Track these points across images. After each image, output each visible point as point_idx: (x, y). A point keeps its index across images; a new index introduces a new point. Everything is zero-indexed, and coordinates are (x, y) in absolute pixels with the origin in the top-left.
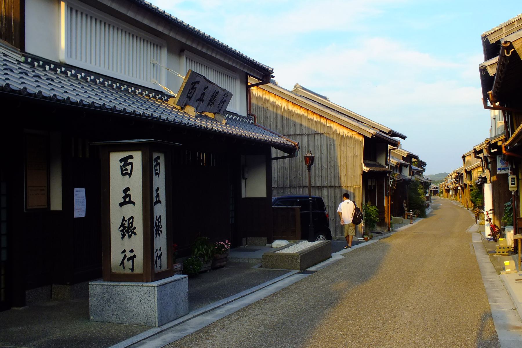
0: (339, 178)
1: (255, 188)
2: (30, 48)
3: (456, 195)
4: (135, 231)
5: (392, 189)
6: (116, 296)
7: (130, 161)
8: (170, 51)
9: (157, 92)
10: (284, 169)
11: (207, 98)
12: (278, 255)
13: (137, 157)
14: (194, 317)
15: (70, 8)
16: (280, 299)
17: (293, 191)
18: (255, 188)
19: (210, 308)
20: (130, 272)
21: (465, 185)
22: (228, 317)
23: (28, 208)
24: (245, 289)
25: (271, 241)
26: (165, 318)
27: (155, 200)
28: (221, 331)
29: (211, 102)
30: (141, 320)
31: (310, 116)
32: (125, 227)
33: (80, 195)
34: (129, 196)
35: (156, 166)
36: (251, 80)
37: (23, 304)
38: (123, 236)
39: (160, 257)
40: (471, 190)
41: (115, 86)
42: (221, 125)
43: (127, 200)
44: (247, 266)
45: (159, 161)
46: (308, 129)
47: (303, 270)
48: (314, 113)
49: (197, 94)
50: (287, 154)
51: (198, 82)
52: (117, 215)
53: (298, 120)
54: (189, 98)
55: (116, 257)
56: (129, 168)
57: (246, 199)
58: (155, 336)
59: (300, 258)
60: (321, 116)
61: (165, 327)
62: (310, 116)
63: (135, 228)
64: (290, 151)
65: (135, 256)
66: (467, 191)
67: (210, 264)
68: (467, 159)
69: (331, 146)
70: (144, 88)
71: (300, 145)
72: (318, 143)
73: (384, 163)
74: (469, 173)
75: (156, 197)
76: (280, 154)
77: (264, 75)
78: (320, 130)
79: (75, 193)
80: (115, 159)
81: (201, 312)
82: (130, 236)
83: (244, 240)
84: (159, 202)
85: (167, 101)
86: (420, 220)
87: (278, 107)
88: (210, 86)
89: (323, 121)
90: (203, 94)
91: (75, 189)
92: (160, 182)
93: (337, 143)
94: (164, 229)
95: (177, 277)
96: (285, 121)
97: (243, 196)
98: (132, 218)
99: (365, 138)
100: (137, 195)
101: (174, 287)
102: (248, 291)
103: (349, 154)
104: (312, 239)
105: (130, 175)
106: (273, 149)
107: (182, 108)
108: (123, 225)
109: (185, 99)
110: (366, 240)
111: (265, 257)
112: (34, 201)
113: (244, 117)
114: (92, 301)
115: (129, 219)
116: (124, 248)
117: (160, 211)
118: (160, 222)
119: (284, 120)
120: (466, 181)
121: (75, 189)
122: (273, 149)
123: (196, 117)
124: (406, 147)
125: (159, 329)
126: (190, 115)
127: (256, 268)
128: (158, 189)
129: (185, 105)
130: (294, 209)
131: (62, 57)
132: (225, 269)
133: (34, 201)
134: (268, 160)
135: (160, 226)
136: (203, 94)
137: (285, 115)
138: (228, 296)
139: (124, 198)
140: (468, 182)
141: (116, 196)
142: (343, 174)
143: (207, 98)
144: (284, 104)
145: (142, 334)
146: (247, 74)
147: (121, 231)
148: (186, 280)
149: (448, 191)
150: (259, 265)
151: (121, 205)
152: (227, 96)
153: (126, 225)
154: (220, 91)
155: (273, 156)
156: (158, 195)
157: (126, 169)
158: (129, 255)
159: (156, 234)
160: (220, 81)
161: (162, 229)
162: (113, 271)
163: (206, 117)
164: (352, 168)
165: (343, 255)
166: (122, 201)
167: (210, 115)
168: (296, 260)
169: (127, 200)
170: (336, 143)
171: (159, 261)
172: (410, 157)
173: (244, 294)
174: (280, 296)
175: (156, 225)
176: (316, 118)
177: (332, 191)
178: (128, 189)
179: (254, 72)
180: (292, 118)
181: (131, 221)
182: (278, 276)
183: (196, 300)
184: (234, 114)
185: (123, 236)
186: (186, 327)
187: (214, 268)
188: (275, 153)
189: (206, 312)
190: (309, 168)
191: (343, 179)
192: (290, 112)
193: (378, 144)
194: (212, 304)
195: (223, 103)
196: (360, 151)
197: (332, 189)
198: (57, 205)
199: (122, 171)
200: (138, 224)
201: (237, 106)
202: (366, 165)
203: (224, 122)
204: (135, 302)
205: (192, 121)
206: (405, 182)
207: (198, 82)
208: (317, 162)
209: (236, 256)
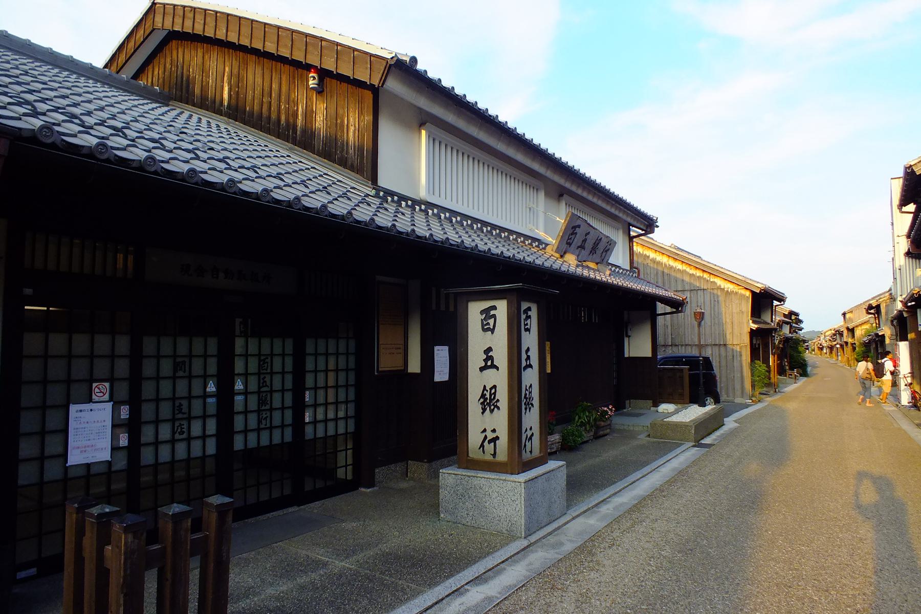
0: (724, 336)
1: (638, 346)
2: (383, 182)
3: (831, 352)
5: (778, 348)
6: (472, 490)
7: (492, 312)
8: (547, 194)
9: (534, 239)
10: (666, 326)
11: (589, 245)
12: (669, 423)
13: (502, 308)
14: (574, 518)
15: (432, 139)
16: (681, 491)
17: (675, 349)
18: (638, 346)
19: (594, 503)
21: (847, 343)
22: (617, 520)
24: (635, 471)
25: (656, 405)
26: (537, 522)
27: (524, 364)
28: (610, 552)
29: (593, 250)
30: (504, 527)
31: (693, 271)
32: (486, 399)
33: (442, 355)
34: (491, 358)
35: (526, 319)
36: (634, 231)
37: (371, 485)
38: (484, 410)
39: (531, 438)
40: (854, 349)
41: (485, 229)
42: (604, 276)
43: (489, 363)
44: (632, 435)
45: (529, 313)
46: (691, 284)
47: (698, 445)
48: (704, 271)
49: (578, 241)
51: (579, 226)
52: (476, 382)
53: (679, 276)
54: (569, 244)
55: (474, 438)
56: (491, 321)
57: (630, 358)
58: (519, 555)
60: (704, 271)
61: (533, 538)
62: (693, 271)
63: (498, 400)
64: (677, 305)
65: (497, 438)
66: (848, 350)
67: (592, 433)
68: (847, 316)
69: (715, 301)
70: (519, 235)
71: (688, 300)
72: (701, 300)
73: (769, 321)
74: (851, 331)
75: (526, 360)
76: (668, 309)
77: (649, 224)
78: (703, 286)
79: (436, 352)
80: (475, 310)
81: (582, 510)
82: (492, 411)
83: (627, 402)
84: (530, 366)
85: (544, 249)
86: (803, 380)
87: (659, 263)
88: (592, 232)
89: (706, 276)
90: (585, 241)
91: (436, 348)
92: (530, 340)
93: (721, 299)
94: (536, 402)
95: (552, 464)
96: (666, 277)
97: (626, 355)
98: (495, 387)
99: (752, 292)
100: (501, 357)
101: (548, 480)
102: (638, 474)
103: (734, 311)
104: (703, 405)
105: (493, 331)
106: (659, 304)
107: (562, 256)
108: (483, 396)
109: (565, 246)
110: (755, 402)
111: (653, 425)
112: (387, 362)
114: (443, 493)
115: (491, 389)
116: (485, 425)
117: (531, 378)
118: (530, 393)
119: (665, 276)
120: (847, 338)
121: (436, 348)
123: (577, 266)
124: (789, 305)
125: (525, 543)
126: (570, 263)
127: (643, 438)
128: (528, 350)
129: (565, 253)
130: (682, 370)
131: (422, 193)
132: (608, 438)
133: (387, 362)
134: (653, 317)
135: (531, 398)
136: (585, 241)
137: (666, 271)
138: (614, 483)
139: (486, 361)
140: (850, 340)
141: (475, 359)
142: (728, 332)
143: (589, 245)
144: (664, 260)
145: (501, 552)
146: (630, 225)
148: (564, 471)
149: (821, 349)
150: (647, 434)
151: (482, 369)
152: (610, 246)
153: (488, 396)
155: (659, 312)
156: (528, 358)
157: (488, 324)
158: (490, 436)
159: (526, 409)
160: (605, 229)
161: (533, 402)
162: (471, 455)
163: (588, 267)
164: (738, 326)
165: (735, 421)
166: (483, 364)
167: (592, 265)
169: (489, 363)
170: (720, 299)
171: (528, 444)
172: (792, 313)
174: (679, 484)
175: (525, 397)
176: (699, 273)
177: (716, 349)
178: (490, 349)
179: (638, 221)
180: (673, 274)
181: (493, 391)
182: (671, 451)
183: (578, 486)
184: (617, 266)
185: (484, 410)
186: (563, 538)
187: (597, 437)
188: (661, 308)
189: (588, 509)
190: (699, 325)
191: (729, 337)
192: (671, 267)
193: (764, 300)
194: (596, 496)
195: (606, 251)
196: (747, 307)
197: (717, 348)
198: (415, 366)
199: (483, 325)
200: (503, 396)
201: (619, 257)
202: (754, 322)
203: (608, 272)
204: (495, 501)
205: (572, 269)
206: (787, 340)
207: (579, 226)
208: (707, 316)
209: (619, 422)
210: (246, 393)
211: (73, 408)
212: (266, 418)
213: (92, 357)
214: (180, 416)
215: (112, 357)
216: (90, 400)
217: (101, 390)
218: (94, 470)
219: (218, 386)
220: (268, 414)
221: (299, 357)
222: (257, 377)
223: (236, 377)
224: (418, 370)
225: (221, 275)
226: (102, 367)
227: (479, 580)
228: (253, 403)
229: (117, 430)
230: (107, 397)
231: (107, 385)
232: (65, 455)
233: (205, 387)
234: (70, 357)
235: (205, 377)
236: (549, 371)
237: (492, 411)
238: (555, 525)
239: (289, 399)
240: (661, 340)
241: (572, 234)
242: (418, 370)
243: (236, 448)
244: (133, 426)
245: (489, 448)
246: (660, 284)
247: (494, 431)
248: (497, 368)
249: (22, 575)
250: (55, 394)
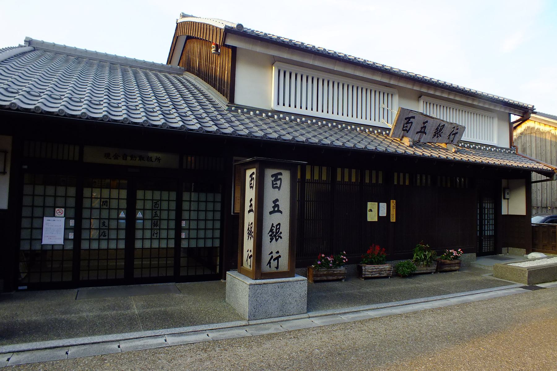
1: (514, 205)
2: (239, 100)
4: (281, 235)
7: (279, 177)
18: (514, 205)
20: (275, 270)
23: (235, 212)
25: (528, 252)
34: (278, 206)
43: (276, 209)
44: (482, 271)
50: (548, 178)
56: (278, 182)
59: (527, 273)
61: (251, 322)
63: (281, 233)
65: (280, 256)
82: (277, 240)
98: (279, 224)
105: (279, 188)
108: (271, 230)
113: (507, 149)
115: (277, 226)
122: (534, 174)
129: (403, 137)
131: (273, 105)
139: (274, 207)
147: (270, 236)
151: (271, 213)
153: (274, 230)
154: (446, 125)
157: (276, 184)
158: (275, 255)
166: (272, 209)
168: (523, 274)
169: (276, 209)
173: (409, 303)
178: (277, 200)
181: (278, 227)
188: (535, 176)
210: (143, 219)
211: (45, 219)
212: (157, 233)
213: (55, 196)
214: (104, 227)
215: (66, 197)
216: (54, 216)
217: (60, 212)
218: (56, 248)
219: (127, 215)
220: (158, 231)
221: (179, 201)
222: (151, 211)
223: (137, 211)
224: (394, 221)
225: (129, 158)
226: (60, 201)
227: (173, 335)
228: (148, 224)
229: (67, 231)
230: (63, 215)
231: (63, 209)
232: (41, 240)
233: (118, 215)
234: (44, 196)
235: (119, 209)
237: (277, 240)
238: (283, 318)
239: (172, 224)
240: (534, 203)
241: (407, 123)
242: (394, 221)
244: (78, 230)
245: (274, 263)
246: (534, 157)
247: (278, 252)
248: (281, 212)
249: (20, 288)
250: (38, 212)
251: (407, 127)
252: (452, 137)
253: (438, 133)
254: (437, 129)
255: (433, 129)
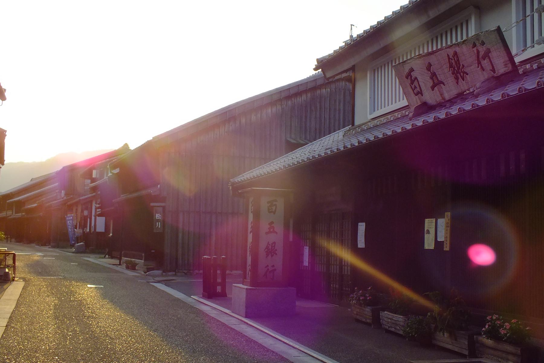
4: (276, 252)
34: (273, 227)
51: (412, 70)
63: (276, 250)
65: (275, 270)
82: (272, 256)
90: (433, 76)
105: (274, 213)
115: (272, 244)
136: (433, 76)
154: (458, 49)
169: (272, 230)
178: (272, 223)
207: (412, 70)
236: (291, 239)
237: (272, 256)
241: (412, 82)
243: (426, 247)
251: (415, 87)
252: (485, 63)
253: (458, 72)
254: (451, 66)
255: (446, 70)
